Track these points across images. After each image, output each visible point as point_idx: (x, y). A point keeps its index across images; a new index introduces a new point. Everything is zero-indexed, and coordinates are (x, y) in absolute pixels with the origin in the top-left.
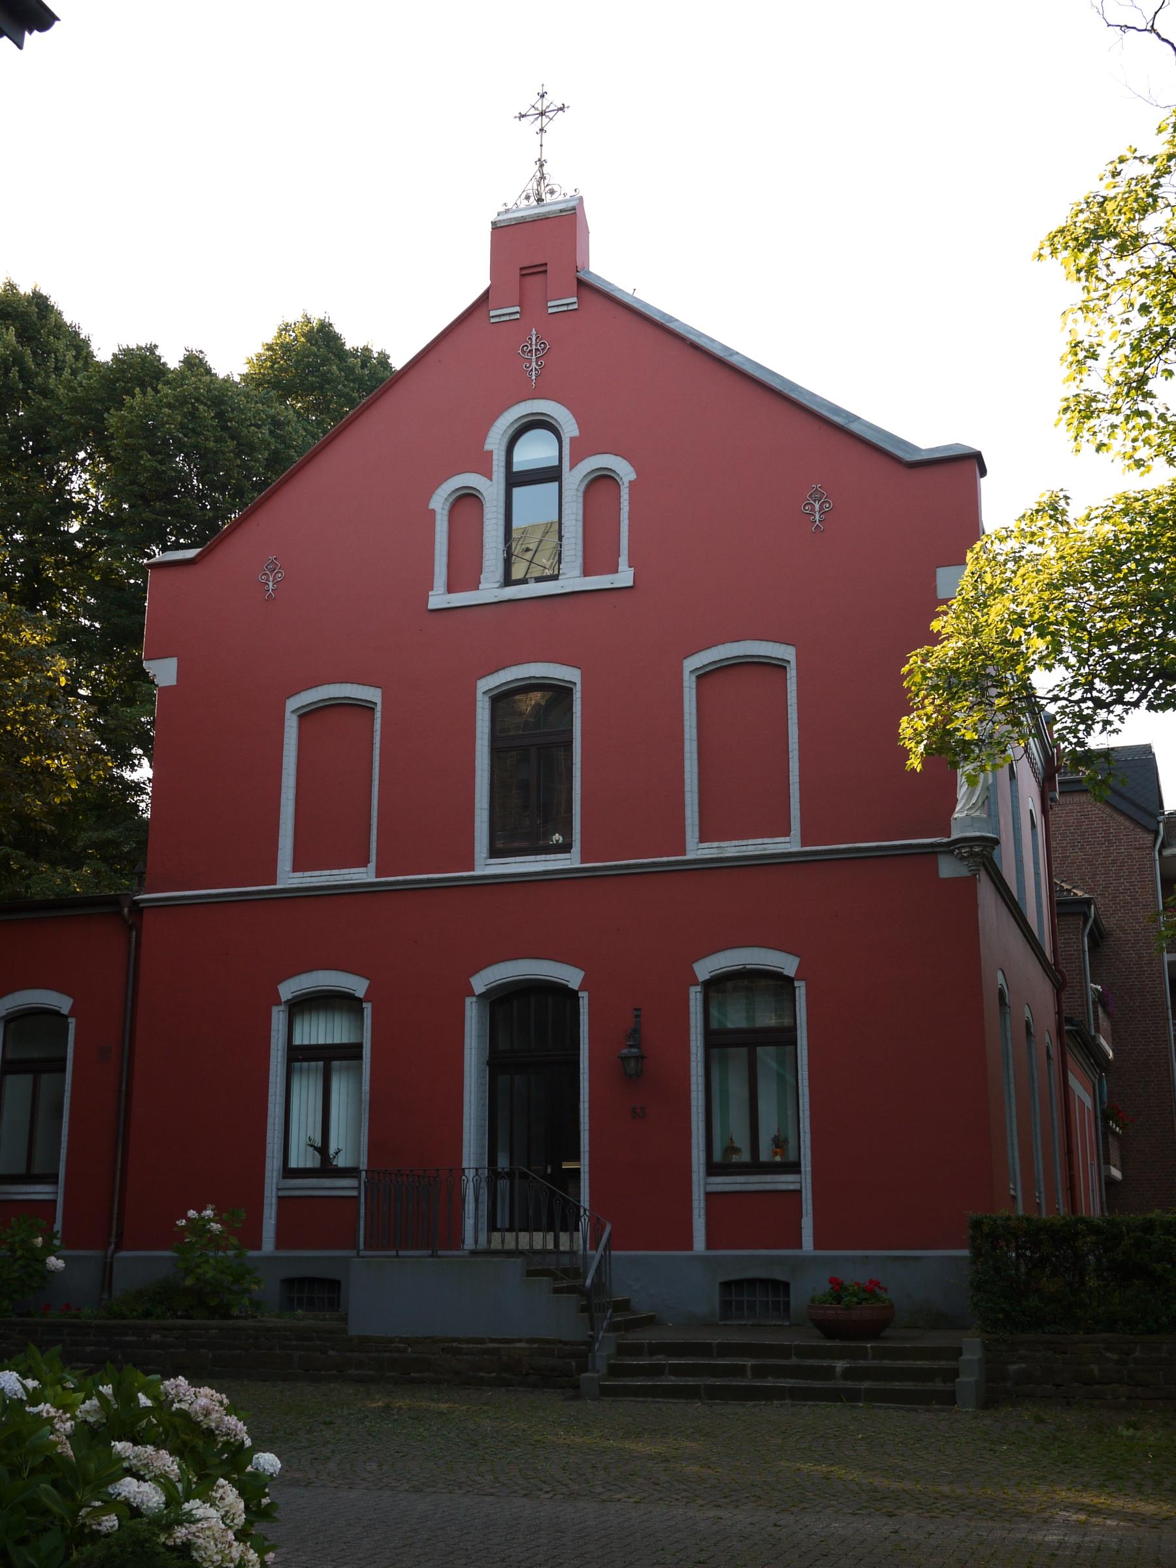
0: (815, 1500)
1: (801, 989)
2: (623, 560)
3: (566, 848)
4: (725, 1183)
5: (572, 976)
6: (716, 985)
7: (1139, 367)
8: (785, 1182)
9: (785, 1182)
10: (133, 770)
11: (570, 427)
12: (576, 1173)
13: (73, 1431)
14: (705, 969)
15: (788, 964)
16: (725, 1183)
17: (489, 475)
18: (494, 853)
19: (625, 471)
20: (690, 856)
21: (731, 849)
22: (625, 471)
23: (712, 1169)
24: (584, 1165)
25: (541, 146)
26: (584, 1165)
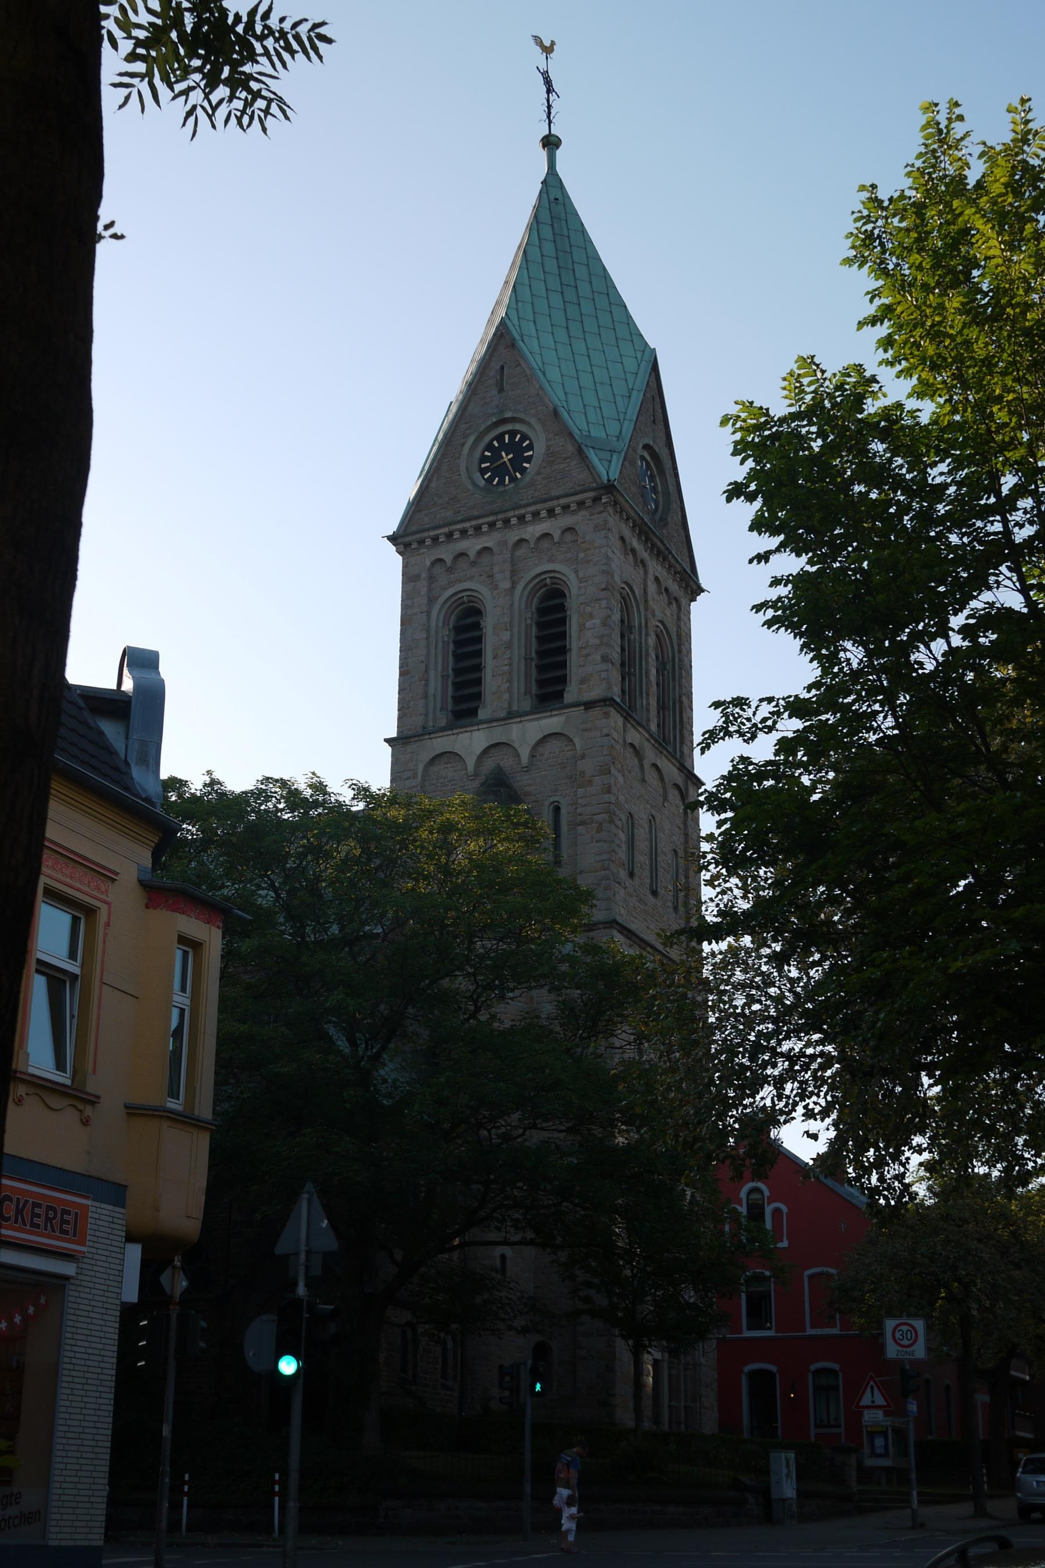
0: (657, 579)
1: (840, 1374)
2: (785, 1238)
3: (770, 1328)
4: (820, 1431)
5: (773, 1368)
6: (818, 1372)
7: (1031, 129)
8: (836, 1430)
9: (836, 1430)
10: (509, 1117)
11: (767, 1193)
12: (777, 1427)
13: (16, 1072)
14: (813, 1367)
15: (836, 1367)
16: (820, 1431)
17: (741, 1205)
18: (749, 1329)
19: (784, 1209)
20: (807, 1333)
21: (820, 1332)
22: (784, 1209)
23: (817, 1426)
24: (779, 1424)
25: (551, 143)
26: (779, 1424)
